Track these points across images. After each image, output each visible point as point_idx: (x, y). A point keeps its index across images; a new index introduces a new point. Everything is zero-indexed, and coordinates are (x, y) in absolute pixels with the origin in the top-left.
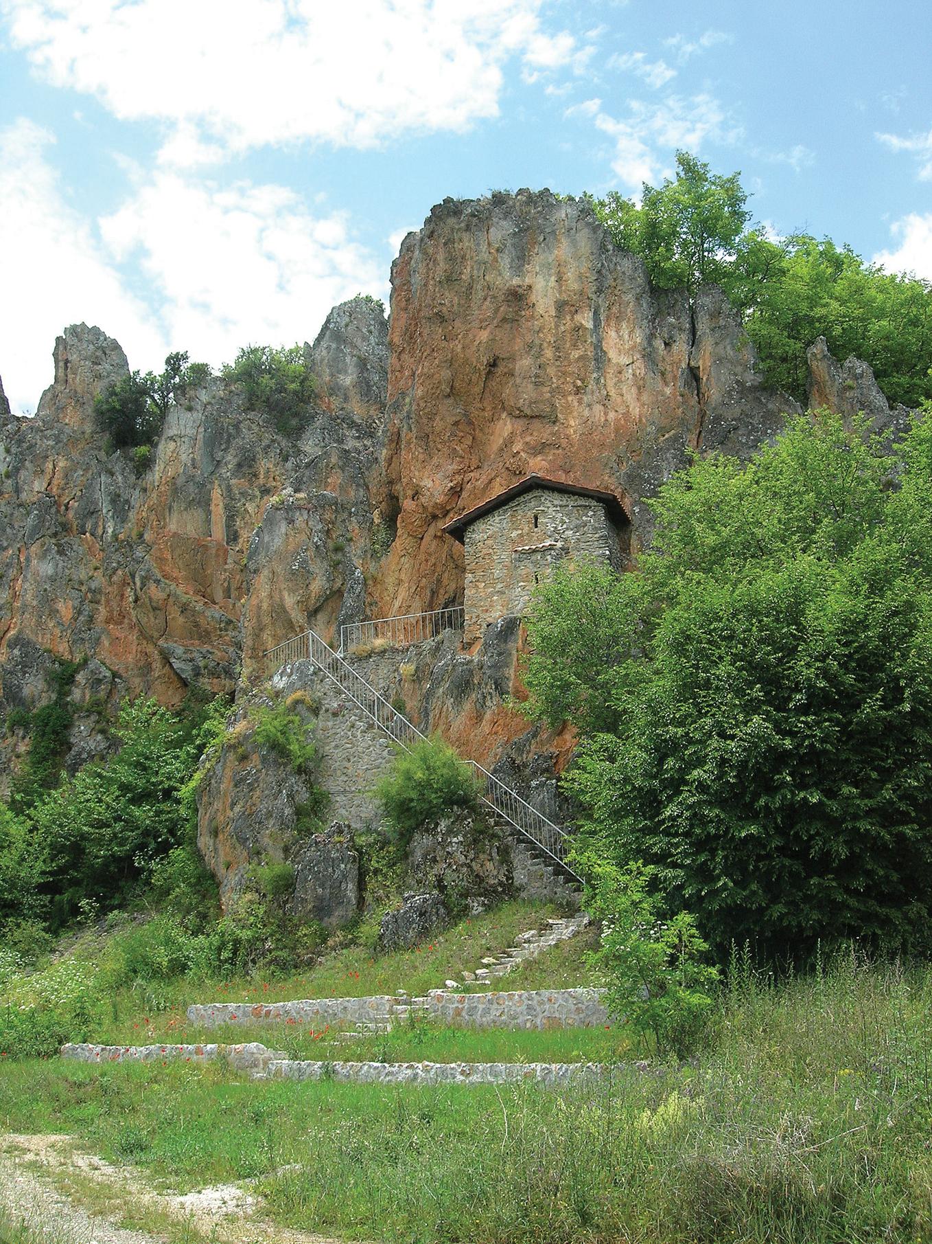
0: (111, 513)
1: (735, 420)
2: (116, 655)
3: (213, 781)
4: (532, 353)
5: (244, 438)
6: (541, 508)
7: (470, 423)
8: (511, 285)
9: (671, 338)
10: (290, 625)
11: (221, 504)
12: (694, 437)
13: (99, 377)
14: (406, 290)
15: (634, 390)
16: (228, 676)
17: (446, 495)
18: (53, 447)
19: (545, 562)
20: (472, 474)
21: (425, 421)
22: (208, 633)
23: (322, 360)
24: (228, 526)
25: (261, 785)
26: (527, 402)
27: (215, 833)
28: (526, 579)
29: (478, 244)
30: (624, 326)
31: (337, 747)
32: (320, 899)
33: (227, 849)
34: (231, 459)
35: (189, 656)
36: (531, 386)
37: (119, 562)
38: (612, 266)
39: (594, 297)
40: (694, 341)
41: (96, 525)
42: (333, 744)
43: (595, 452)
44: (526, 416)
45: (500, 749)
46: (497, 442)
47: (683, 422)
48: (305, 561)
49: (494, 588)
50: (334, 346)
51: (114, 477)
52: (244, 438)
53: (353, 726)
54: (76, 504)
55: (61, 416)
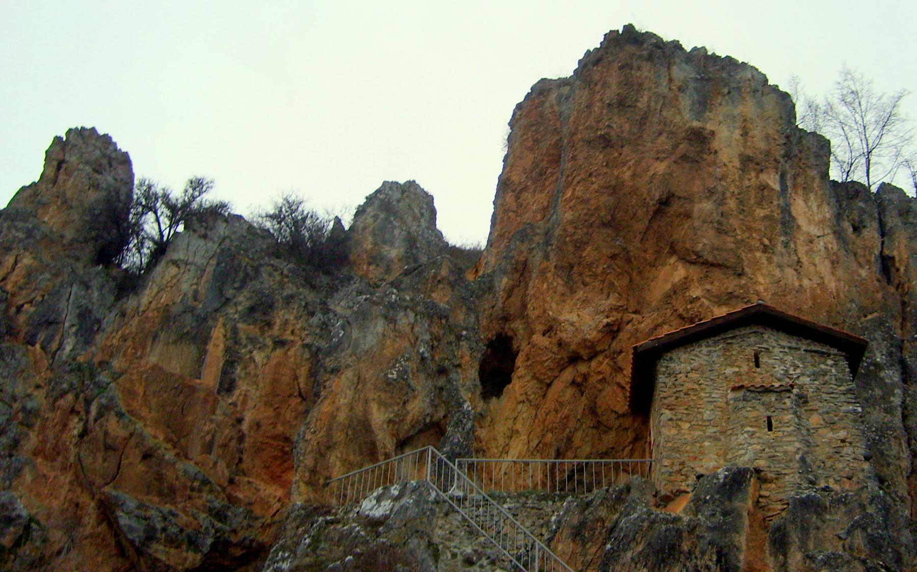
0: (74, 329)
2: (38, 495)
4: (714, 198)
6: (765, 345)
7: (628, 260)
10: (371, 452)
12: (898, 324)
13: (96, 186)
15: (827, 263)
17: (600, 331)
18: (21, 241)
19: (783, 406)
21: (570, 248)
22: (172, 490)
23: (364, 228)
24: (224, 372)
26: (708, 247)
28: (755, 424)
29: (659, 77)
30: (812, 198)
34: (243, 300)
35: (141, 512)
37: (71, 385)
39: (782, 161)
41: (50, 339)
44: (706, 263)
50: (382, 216)
51: (90, 291)
54: (32, 309)
55: (40, 211)
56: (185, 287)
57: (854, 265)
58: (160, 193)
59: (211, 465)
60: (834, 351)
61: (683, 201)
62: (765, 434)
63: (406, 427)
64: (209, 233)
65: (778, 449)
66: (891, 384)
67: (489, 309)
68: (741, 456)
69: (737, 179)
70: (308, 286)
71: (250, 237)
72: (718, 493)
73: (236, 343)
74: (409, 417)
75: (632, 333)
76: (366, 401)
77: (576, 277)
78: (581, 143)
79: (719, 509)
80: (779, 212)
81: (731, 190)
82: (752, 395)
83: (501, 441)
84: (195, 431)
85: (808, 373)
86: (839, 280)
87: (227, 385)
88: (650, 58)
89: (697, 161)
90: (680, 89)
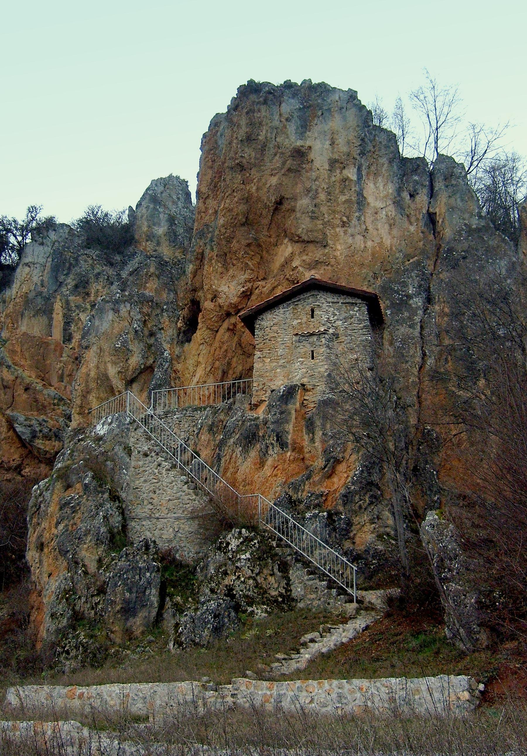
1: (464, 252)
3: (42, 506)
4: (310, 195)
5: (81, 267)
7: (259, 246)
8: (296, 146)
9: (415, 191)
10: (112, 391)
11: (61, 313)
12: (432, 262)
14: (212, 154)
15: (387, 227)
16: (58, 439)
17: (239, 297)
19: (320, 344)
20: (259, 283)
21: (224, 243)
24: (65, 330)
25: (82, 508)
26: (305, 231)
27: (41, 547)
29: (272, 114)
30: (380, 181)
31: (145, 481)
32: (126, 602)
33: (50, 561)
34: (71, 282)
35: (28, 423)
36: (308, 219)
38: (372, 137)
39: (358, 157)
40: (432, 194)
42: (142, 479)
43: (356, 269)
44: (303, 241)
45: (279, 488)
46: (279, 260)
47: (423, 252)
48: (126, 342)
49: (278, 363)
50: (152, 206)
52: (81, 267)
53: (159, 465)
56: (35, 279)
57: (406, 224)
58: (11, 219)
59: (63, 389)
60: (359, 301)
61: (290, 200)
62: (309, 362)
63: (130, 373)
64: (44, 241)
65: (315, 371)
66: (416, 307)
67: (184, 285)
68: (296, 376)
69: (327, 178)
70: (108, 264)
71: (70, 238)
72: (279, 401)
73: (69, 310)
74: (131, 367)
75: (258, 295)
76: (105, 363)
77: (228, 260)
78: (227, 170)
79: (278, 411)
80: (355, 195)
81: (322, 187)
82: (304, 338)
83: (191, 369)
84: (52, 369)
85: (341, 318)
86: (394, 237)
87: (68, 338)
88: (265, 102)
89: (299, 171)
90: (287, 120)
